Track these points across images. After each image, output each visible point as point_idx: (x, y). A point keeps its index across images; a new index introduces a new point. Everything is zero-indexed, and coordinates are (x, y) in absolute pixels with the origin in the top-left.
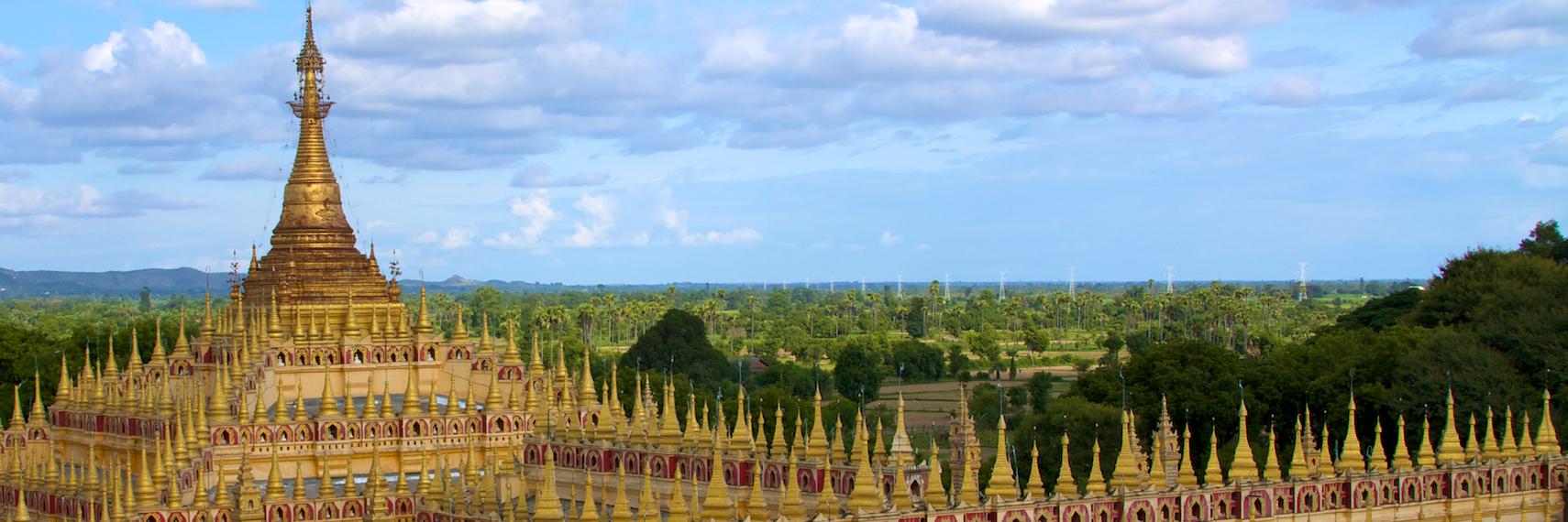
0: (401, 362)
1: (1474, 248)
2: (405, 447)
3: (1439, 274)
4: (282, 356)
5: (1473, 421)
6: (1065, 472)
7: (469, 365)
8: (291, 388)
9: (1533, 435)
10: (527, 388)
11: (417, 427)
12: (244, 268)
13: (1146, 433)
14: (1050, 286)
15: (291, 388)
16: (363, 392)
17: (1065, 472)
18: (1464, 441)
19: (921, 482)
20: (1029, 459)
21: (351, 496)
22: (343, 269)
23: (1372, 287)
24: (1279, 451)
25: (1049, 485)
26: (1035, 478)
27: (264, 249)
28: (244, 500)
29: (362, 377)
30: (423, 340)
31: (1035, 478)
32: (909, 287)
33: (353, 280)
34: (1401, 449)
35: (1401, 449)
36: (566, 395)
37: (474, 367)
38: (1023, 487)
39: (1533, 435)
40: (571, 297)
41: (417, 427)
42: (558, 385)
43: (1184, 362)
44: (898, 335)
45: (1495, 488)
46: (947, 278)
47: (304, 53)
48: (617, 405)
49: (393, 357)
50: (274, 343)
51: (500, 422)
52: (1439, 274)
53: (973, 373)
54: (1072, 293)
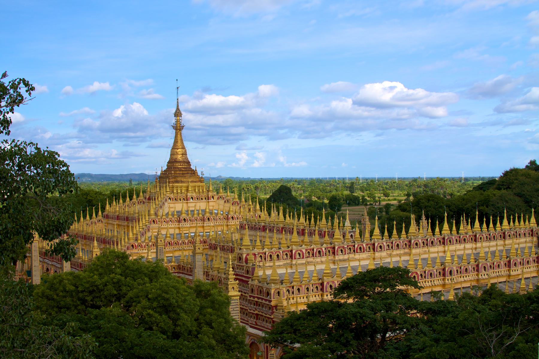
0: (204, 200)
1: (512, 168)
2: (205, 225)
3: (502, 175)
4: (170, 198)
5: (512, 217)
6: (395, 232)
7: (223, 201)
8: (172, 208)
9: (529, 221)
10: (240, 207)
11: (208, 219)
12: (159, 173)
13: (418, 220)
14: (390, 178)
15: (172, 208)
16: (193, 209)
17: (395, 232)
18: (509, 223)
19: (353, 235)
20: (384, 228)
21: (190, 239)
22: (187, 173)
23: (483, 179)
24: (456, 226)
25: (390, 236)
26: (386, 233)
27: (165, 168)
28: (159, 240)
29: (193, 205)
30: (189, 195)
31: (386, 233)
32: (350, 179)
33: (190, 177)
34: (491, 225)
35: (491, 225)
36: (252, 210)
37: (225, 202)
38: (383, 236)
39: (529, 221)
40: (253, 181)
41: (208, 219)
42: (249, 207)
43: (429, 200)
44: (347, 192)
45: (518, 236)
46: (361, 176)
47: (176, 112)
48: (266, 213)
49: (202, 199)
50: (168, 195)
51: (232, 218)
52: (502, 175)
53: (368, 203)
54: (397, 181)
